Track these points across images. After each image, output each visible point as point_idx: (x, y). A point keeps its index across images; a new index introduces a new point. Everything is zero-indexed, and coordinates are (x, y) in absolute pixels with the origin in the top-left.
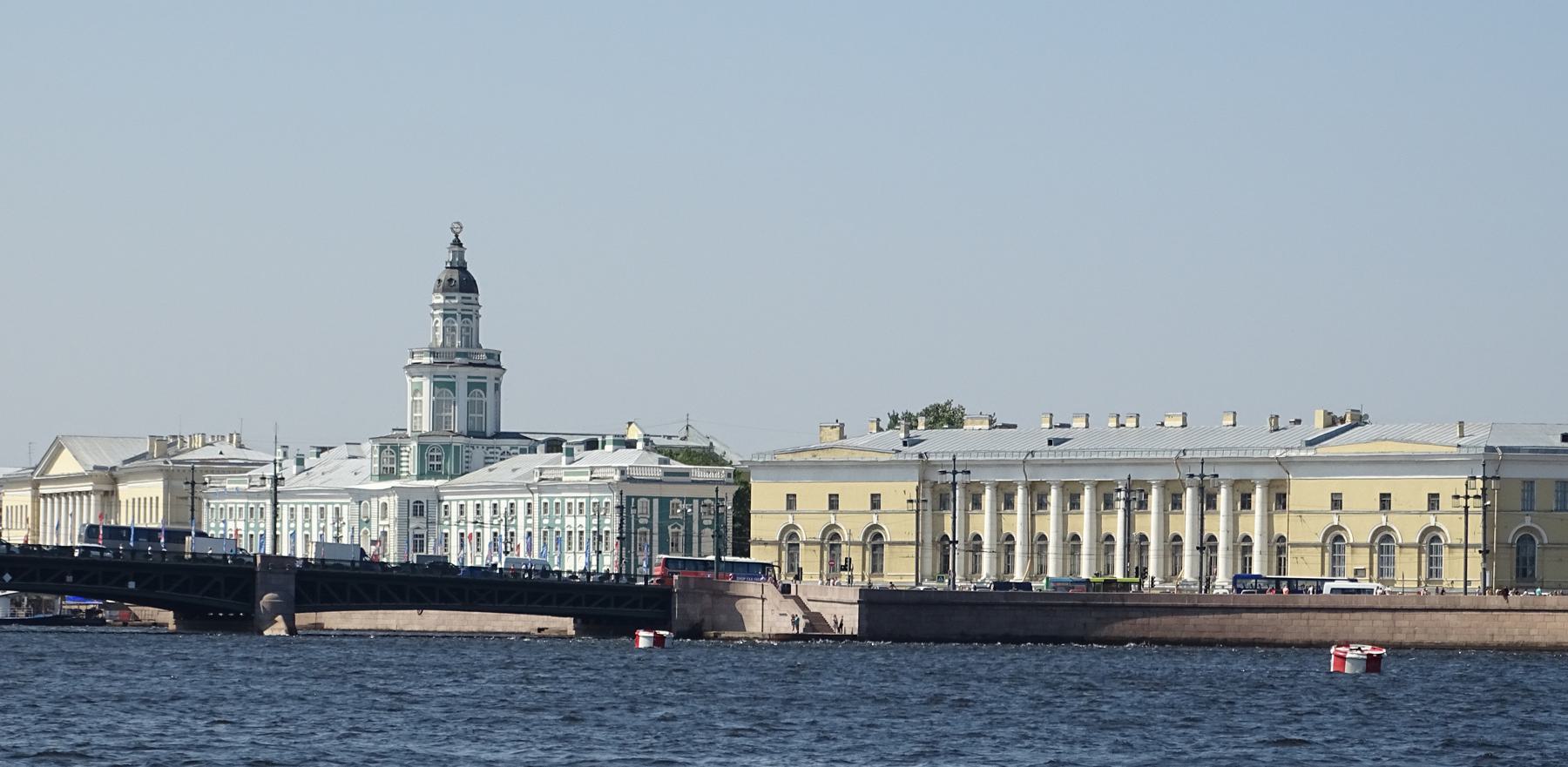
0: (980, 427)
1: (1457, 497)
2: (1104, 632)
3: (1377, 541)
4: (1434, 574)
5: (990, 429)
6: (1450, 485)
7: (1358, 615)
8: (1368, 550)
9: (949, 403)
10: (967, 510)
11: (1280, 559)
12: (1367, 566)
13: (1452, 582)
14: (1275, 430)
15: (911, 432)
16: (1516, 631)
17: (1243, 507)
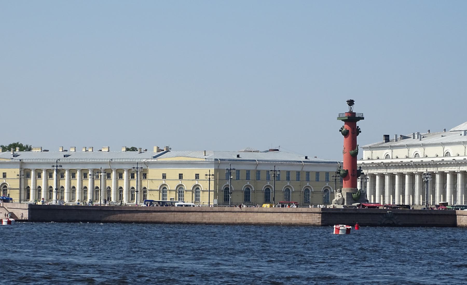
0: (38, 151)
1: (207, 175)
2: (107, 218)
3: (178, 189)
4: (197, 200)
5: (126, 151)
6: (203, 172)
7: (191, 213)
8: (175, 192)
9: (18, 143)
10: (105, 178)
11: (120, 194)
12: (175, 197)
13: (204, 203)
14: (140, 153)
15: (15, 152)
16: (244, 219)
17: (132, 178)
